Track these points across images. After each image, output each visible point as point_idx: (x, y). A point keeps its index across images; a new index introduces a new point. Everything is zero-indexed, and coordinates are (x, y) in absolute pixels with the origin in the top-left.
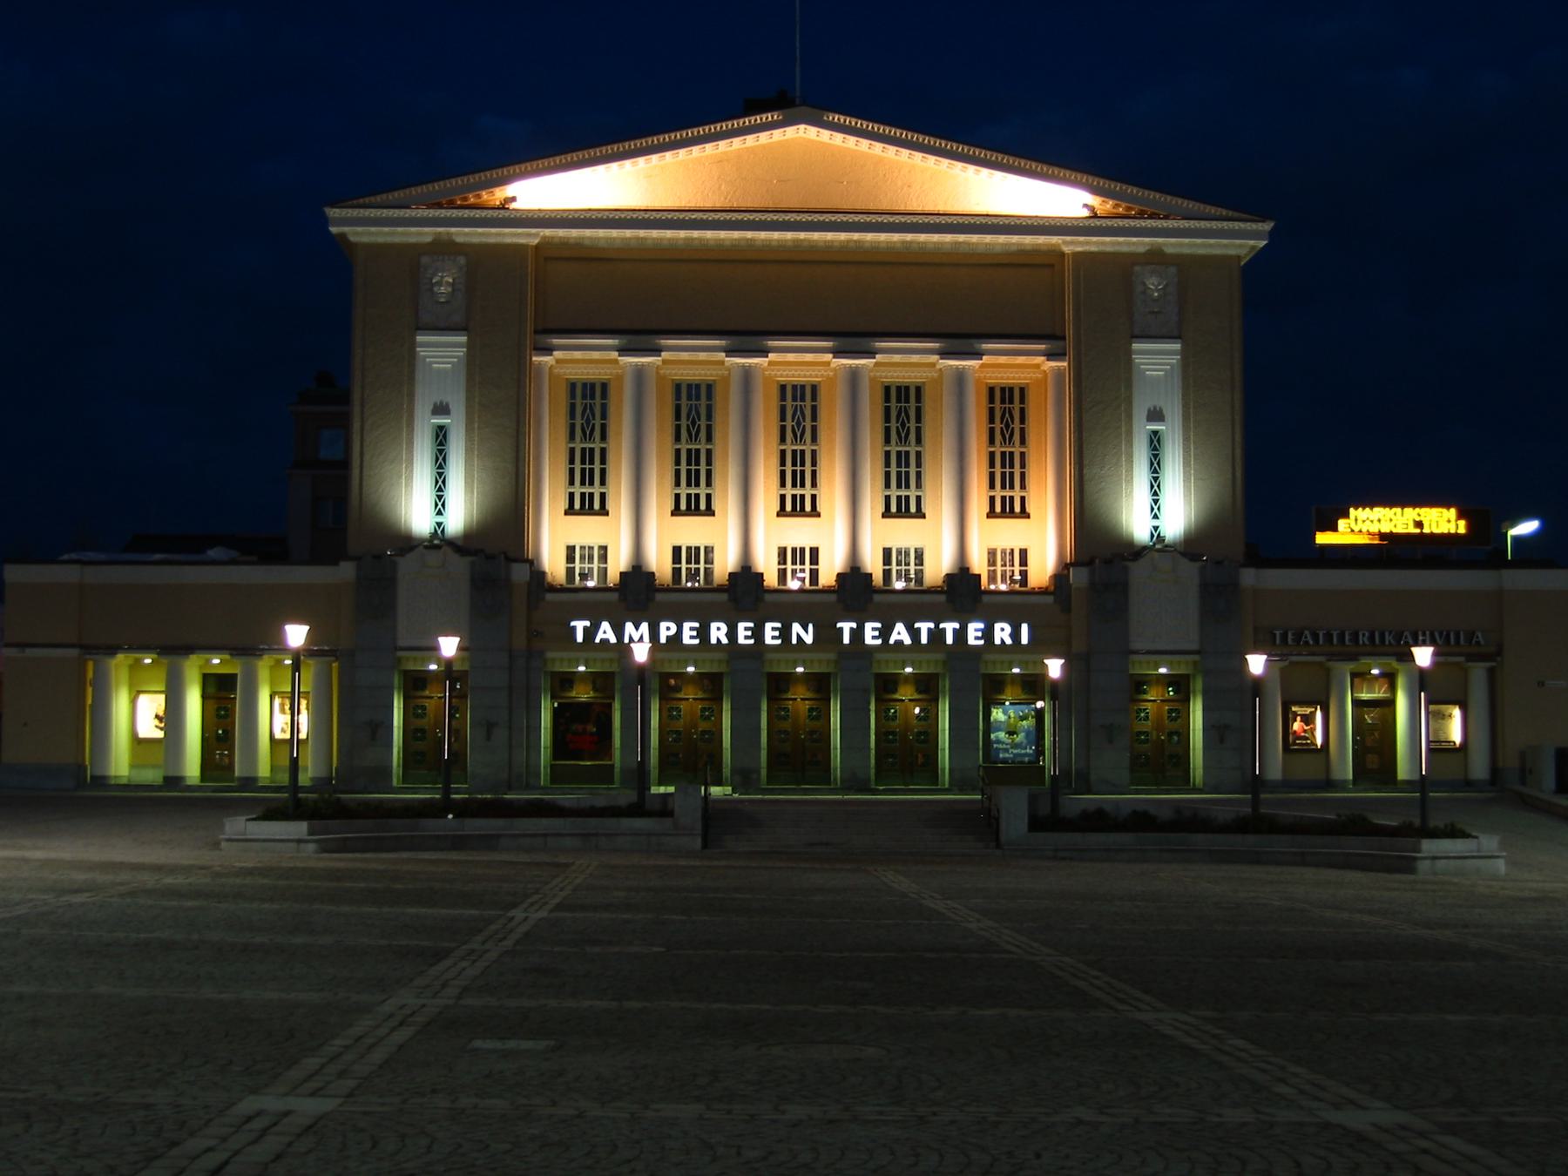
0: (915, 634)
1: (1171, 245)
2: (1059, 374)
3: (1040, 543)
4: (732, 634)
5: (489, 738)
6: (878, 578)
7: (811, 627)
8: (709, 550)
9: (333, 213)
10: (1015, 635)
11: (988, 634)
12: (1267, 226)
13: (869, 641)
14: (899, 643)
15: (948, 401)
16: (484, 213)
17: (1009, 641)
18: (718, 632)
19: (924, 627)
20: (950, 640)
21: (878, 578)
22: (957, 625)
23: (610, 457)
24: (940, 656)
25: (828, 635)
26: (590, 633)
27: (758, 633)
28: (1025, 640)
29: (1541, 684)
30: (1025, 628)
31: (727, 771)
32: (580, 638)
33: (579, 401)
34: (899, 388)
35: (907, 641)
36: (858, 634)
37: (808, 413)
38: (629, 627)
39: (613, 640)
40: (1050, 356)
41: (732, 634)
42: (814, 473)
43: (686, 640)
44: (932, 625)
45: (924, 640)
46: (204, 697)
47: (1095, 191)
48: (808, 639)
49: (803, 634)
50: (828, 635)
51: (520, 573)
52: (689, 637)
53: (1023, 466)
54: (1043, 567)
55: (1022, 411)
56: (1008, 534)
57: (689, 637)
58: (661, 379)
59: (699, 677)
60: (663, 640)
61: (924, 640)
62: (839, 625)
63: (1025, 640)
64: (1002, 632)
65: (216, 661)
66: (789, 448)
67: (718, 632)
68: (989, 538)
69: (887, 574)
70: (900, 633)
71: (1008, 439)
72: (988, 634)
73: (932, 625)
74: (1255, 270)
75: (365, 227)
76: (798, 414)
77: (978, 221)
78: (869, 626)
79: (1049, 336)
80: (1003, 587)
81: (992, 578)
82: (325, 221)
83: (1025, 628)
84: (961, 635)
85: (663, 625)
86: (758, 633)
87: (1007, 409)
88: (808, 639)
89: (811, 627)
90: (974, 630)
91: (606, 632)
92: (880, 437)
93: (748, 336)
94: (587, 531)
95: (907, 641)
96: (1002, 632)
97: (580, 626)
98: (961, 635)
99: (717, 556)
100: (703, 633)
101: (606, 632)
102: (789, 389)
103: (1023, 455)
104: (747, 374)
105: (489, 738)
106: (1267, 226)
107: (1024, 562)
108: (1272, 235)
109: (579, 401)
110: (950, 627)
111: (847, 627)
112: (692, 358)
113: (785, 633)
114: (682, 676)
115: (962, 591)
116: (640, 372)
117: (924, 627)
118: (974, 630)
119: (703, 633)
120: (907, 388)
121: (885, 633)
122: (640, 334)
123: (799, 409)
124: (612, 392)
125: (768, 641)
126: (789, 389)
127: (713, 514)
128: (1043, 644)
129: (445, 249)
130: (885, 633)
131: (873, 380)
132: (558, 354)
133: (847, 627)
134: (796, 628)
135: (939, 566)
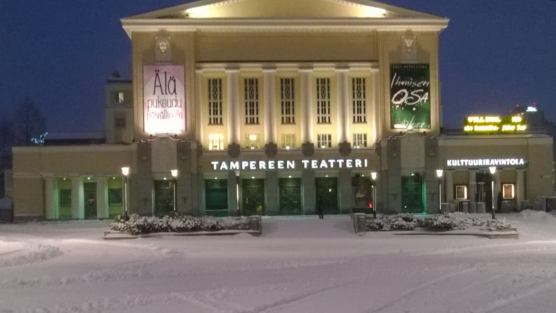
0: (329, 164)
1: (415, 28)
2: (376, 74)
3: (371, 132)
4: (267, 165)
5: (185, 202)
6: (316, 145)
7: (293, 162)
8: (294, 136)
9: (123, 21)
10: (363, 163)
11: (353, 163)
12: (447, 21)
13: (313, 167)
14: (324, 167)
15: (338, 84)
16: (352, 21)
17: (360, 166)
18: (262, 165)
19: (332, 161)
20: (340, 166)
21: (316, 145)
22: (308, 161)
23: (223, 105)
24: (338, 171)
25: (299, 165)
26: (219, 166)
27: (276, 165)
28: (366, 165)
29: (542, 177)
30: (366, 161)
31: (425, 209)
32: (215, 168)
33: (284, 85)
34: (357, 79)
35: (326, 166)
36: (310, 165)
37: (255, 89)
38: (232, 163)
39: (226, 168)
40: (373, 67)
41: (267, 165)
42: (365, 109)
43: (251, 168)
44: (334, 161)
45: (332, 166)
46: (85, 191)
47: (387, 9)
48: (293, 166)
49: (291, 165)
50: (299, 165)
51: (194, 146)
52: (349, 164)
53: (329, 105)
54: (372, 139)
55: (328, 87)
56: (360, 129)
57: (252, 166)
58: (240, 78)
59: (292, 179)
60: (243, 168)
61: (332, 166)
62: (212, 163)
63: (366, 165)
64: (358, 163)
65: (89, 178)
66: (212, 102)
67: (262, 165)
68: (353, 131)
69: (319, 144)
70: (324, 164)
71: (288, 96)
72: (353, 163)
73: (334, 161)
74: (442, 35)
75: (132, 27)
76: (251, 90)
77: (198, 21)
78: (348, 161)
79: (374, 61)
80: (358, 147)
81: (355, 144)
82: (120, 24)
83: (366, 161)
84: (344, 164)
85: (243, 163)
86: (276, 165)
87: (359, 85)
88: (293, 166)
89: (293, 162)
90: (280, 164)
91: (224, 166)
92: (244, 97)
93: (307, 62)
94: (324, 129)
95: (326, 166)
96: (358, 163)
97: (215, 163)
98: (344, 164)
99: (368, 138)
100: (257, 165)
101: (224, 166)
102: (284, 81)
103: (364, 102)
104: (342, 76)
105: (185, 202)
106: (447, 21)
107: (365, 138)
108: (449, 23)
109: (320, 85)
110: (340, 161)
111: (306, 162)
112: (287, 70)
113: (285, 165)
114: (288, 179)
115: (345, 149)
116: (270, 74)
117: (332, 161)
118: (280, 164)
119: (257, 165)
120: (324, 80)
121: (319, 164)
122: (342, 62)
123: (323, 86)
124: (223, 82)
125: (279, 167)
126: (284, 81)
127: (295, 124)
128: (371, 167)
129: (163, 34)
130: (319, 164)
131: (349, 77)
132: (204, 70)
133: (306, 162)
134: (289, 163)
135: (337, 140)
